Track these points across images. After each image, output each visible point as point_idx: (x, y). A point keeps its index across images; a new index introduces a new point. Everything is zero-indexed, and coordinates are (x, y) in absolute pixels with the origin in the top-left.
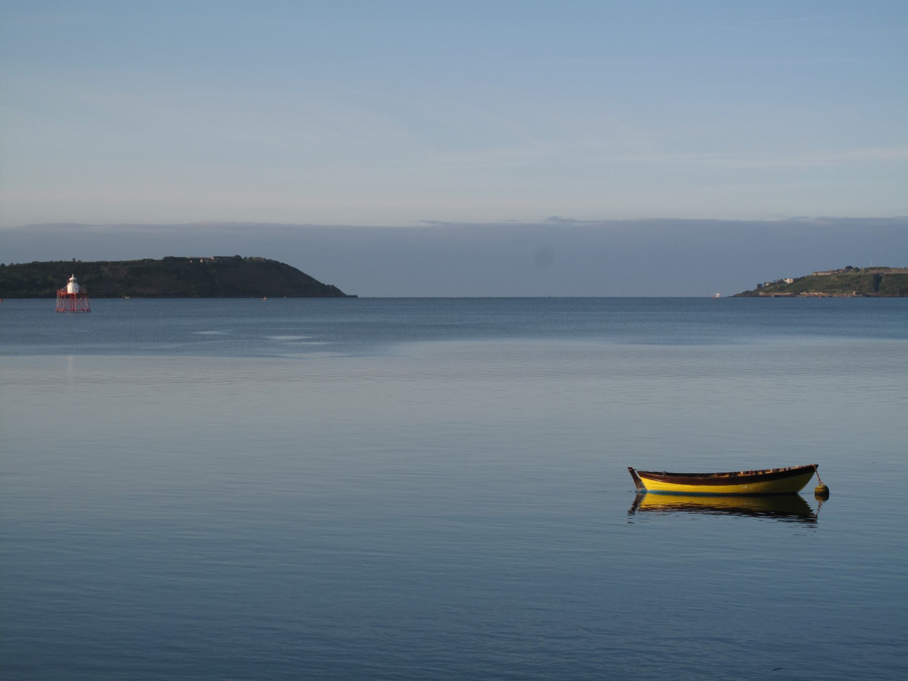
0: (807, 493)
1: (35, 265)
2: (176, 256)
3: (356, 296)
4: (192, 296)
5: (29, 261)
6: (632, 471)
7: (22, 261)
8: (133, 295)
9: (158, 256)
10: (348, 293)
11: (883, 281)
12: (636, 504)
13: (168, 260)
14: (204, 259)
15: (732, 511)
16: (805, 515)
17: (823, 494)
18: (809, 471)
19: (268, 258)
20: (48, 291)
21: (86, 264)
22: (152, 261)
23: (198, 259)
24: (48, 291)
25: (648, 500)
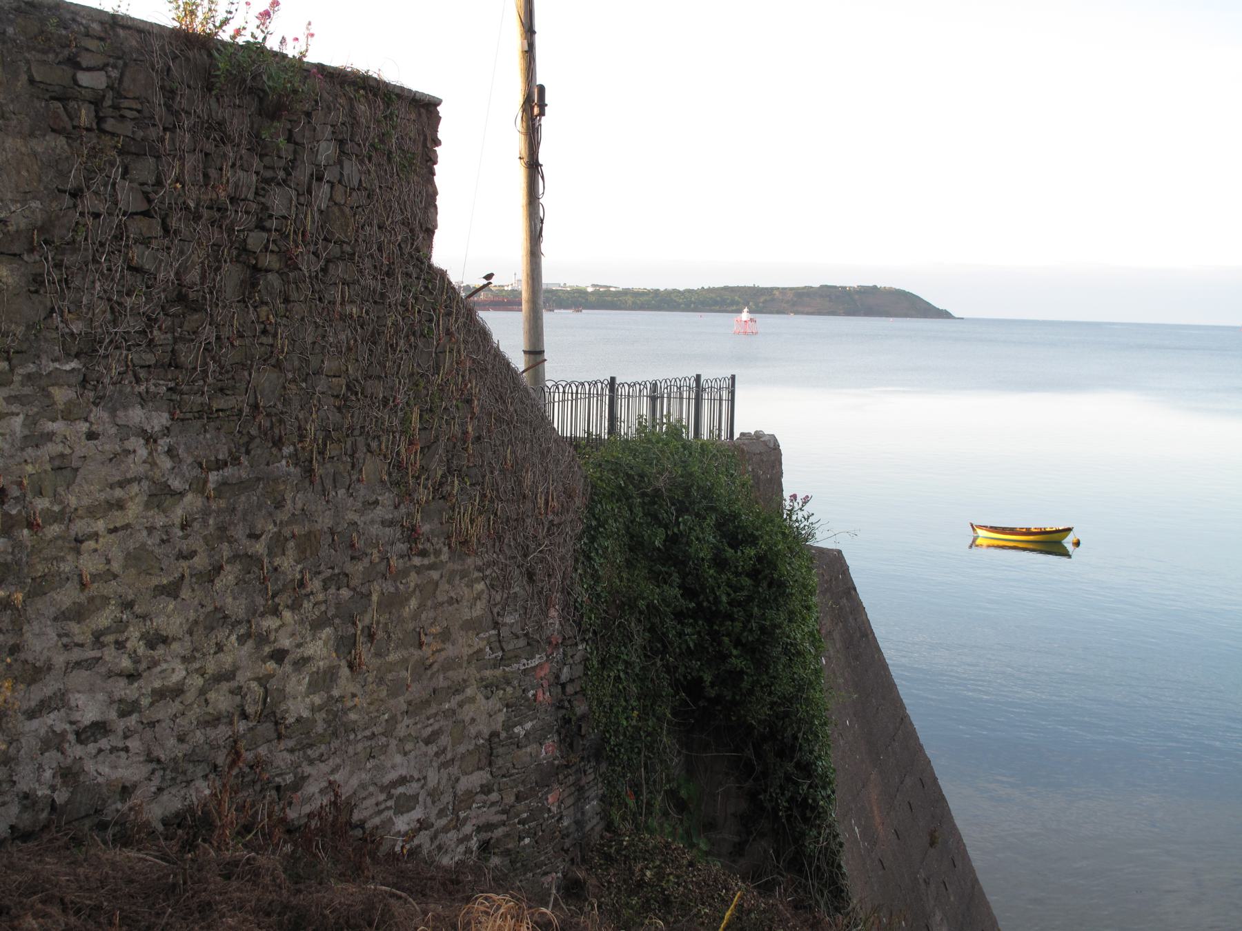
0: (1068, 542)
1: (726, 289)
2: (829, 284)
3: (963, 318)
4: (839, 315)
5: (722, 285)
6: (972, 525)
7: (717, 286)
8: (796, 313)
9: (816, 284)
10: (957, 316)
11: (448, 835)
12: (974, 541)
13: (823, 287)
14: (850, 287)
15: (1024, 549)
16: (1065, 553)
17: (1077, 544)
18: (1069, 530)
19: (897, 288)
20: (734, 308)
21: (763, 289)
22: (811, 287)
23: (845, 288)
24: (734, 308)
25: (979, 542)
